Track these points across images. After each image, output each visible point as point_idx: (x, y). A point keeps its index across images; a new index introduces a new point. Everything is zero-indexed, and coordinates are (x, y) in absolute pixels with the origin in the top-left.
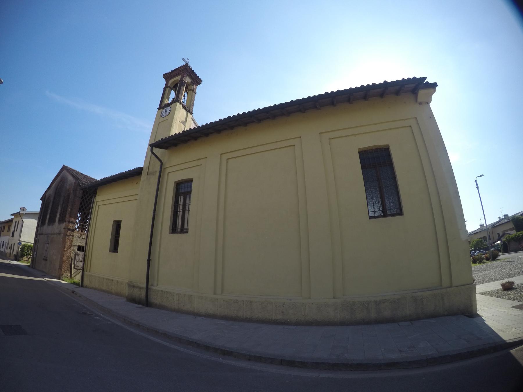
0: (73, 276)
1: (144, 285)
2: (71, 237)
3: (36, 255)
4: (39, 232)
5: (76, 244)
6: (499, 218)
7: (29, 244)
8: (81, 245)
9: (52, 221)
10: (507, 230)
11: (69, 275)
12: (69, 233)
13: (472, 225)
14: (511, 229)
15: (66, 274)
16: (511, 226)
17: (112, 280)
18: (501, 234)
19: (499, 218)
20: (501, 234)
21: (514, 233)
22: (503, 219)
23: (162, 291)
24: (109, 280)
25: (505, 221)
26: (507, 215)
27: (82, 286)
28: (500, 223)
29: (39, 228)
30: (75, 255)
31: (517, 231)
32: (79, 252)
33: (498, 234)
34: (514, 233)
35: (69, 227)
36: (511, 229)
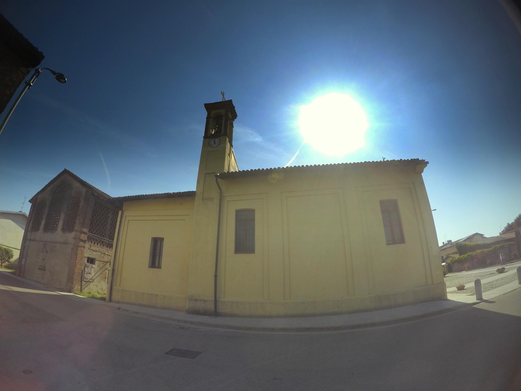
0: (83, 288)
1: (213, 299)
2: (82, 248)
3: (25, 262)
4: (28, 237)
5: (86, 256)
6: (443, 243)
7: (4, 247)
8: (90, 256)
9: (50, 227)
10: (450, 254)
11: (79, 287)
12: (81, 244)
13: (441, 241)
14: (454, 253)
15: (77, 287)
16: (455, 250)
17: (157, 295)
18: (444, 257)
19: (443, 243)
20: (444, 257)
21: (457, 256)
22: (446, 244)
23: (231, 302)
24: (152, 294)
25: (449, 246)
26: (450, 241)
27: (110, 300)
28: (444, 247)
29: (29, 233)
30: (85, 267)
31: (460, 255)
32: (88, 264)
33: (442, 257)
34: (457, 256)
35: (81, 238)
36: (454, 253)
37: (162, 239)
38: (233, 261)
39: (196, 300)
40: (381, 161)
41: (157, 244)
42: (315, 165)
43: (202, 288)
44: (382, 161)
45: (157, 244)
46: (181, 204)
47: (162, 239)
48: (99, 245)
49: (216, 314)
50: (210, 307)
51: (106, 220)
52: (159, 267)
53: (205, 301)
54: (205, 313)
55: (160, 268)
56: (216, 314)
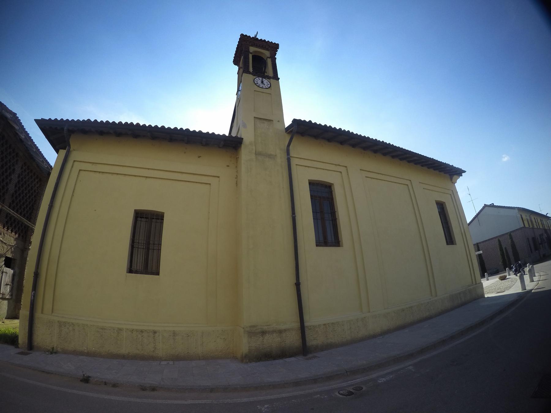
17: (155, 332)
23: (324, 325)
24: (142, 331)
37: (159, 217)
38: (313, 254)
39: (263, 333)
40: (224, 135)
41: (147, 228)
42: (176, 128)
43: (268, 306)
44: (227, 135)
45: (147, 228)
46: (185, 153)
47: (159, 217)
48: (10, 231)
49: (304, 350)
50: (292, 339)
51: (10, 174)
52: (474, 245)
53: (280, 332)
54: (283, 354)
55: (158, 274)
56: (304, 350)
